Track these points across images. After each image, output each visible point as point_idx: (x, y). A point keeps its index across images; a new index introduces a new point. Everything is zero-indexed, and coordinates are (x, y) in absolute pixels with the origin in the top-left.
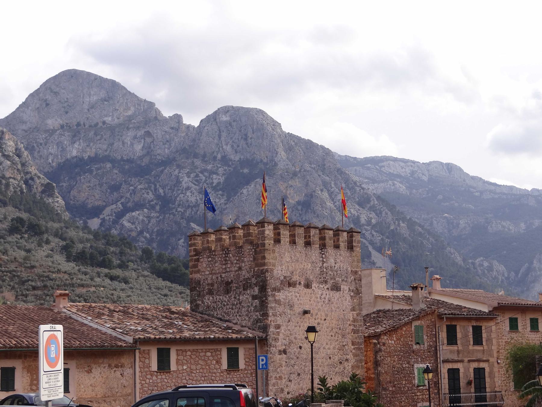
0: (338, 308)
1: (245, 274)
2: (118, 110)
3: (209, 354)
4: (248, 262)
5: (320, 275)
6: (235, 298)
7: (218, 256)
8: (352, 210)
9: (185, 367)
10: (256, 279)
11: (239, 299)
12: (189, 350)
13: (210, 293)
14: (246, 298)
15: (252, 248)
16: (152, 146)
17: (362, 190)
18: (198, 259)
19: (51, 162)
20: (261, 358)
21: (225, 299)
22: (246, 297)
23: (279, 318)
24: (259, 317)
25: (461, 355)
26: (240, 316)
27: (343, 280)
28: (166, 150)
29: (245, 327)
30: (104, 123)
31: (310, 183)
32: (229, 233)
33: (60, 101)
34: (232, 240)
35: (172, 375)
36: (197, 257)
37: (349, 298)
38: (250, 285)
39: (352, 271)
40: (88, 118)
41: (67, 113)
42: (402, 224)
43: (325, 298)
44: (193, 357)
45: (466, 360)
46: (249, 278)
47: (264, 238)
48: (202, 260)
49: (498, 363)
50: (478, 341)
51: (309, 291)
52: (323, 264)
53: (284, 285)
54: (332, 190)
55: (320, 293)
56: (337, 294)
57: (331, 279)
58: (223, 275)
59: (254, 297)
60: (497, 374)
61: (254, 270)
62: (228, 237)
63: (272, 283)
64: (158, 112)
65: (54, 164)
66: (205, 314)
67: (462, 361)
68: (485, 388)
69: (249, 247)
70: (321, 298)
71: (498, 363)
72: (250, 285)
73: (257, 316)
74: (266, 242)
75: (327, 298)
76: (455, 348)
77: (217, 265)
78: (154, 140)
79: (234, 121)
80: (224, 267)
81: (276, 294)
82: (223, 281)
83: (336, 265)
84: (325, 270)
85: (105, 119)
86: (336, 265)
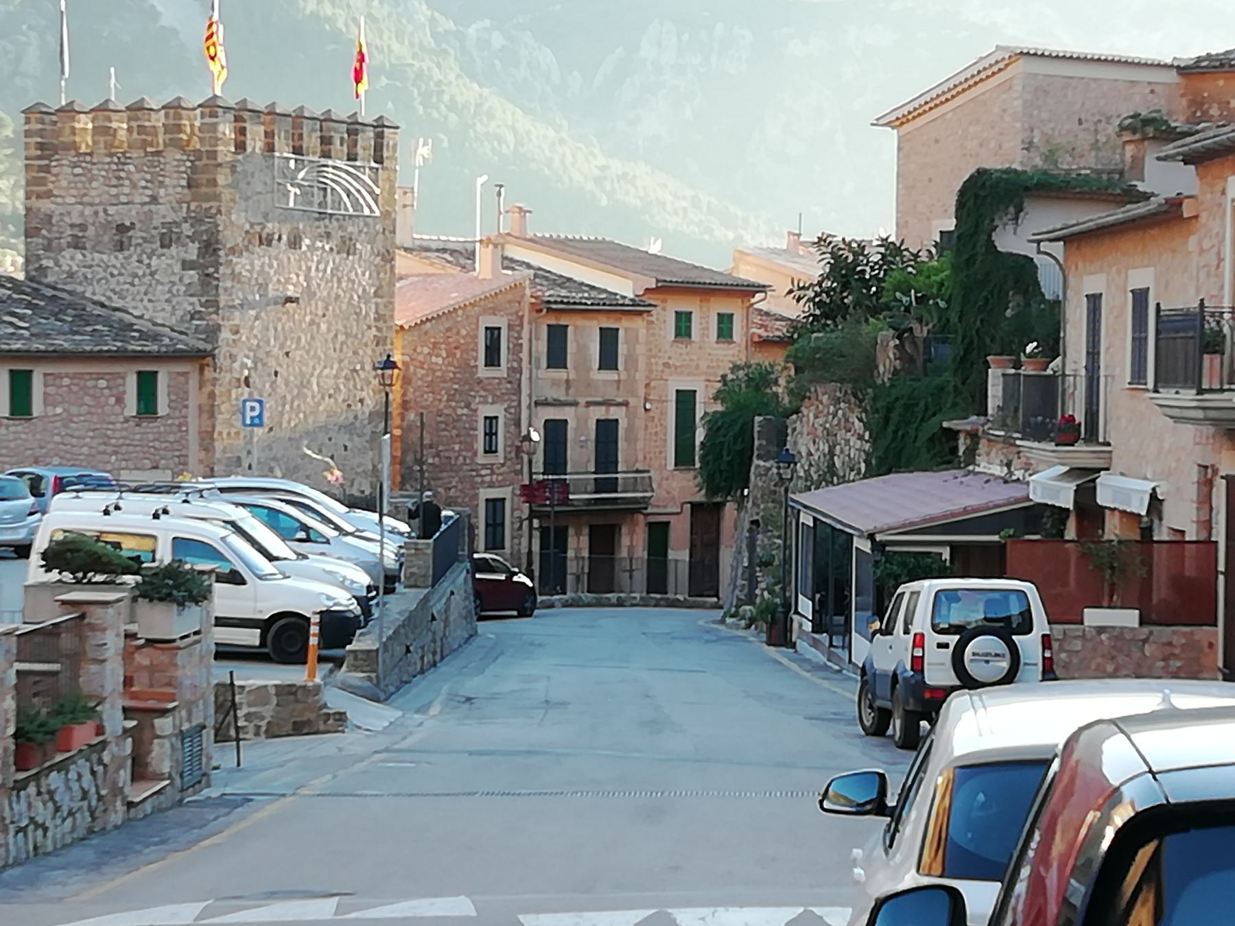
1: (164, 213)
3: (102, 383)
4: (175, 187)
6: (140, 261)
7: (100, 166)
9: (59, 410)
10: (192, 226)
11: (149, 266)
12: (67, 376)
13: (77, 244)
14: (169, 265)
15: (185, 158)
18: (48, 166)
20: (248, 404)
21: (116, 259)
22: (167, 262)
24: (199, 308)
25: (571, 391)
29: (163, 325)
32: (129, 119)
34: (135, 135)
35: (35, 424)
36: (46, 162)
44: (75, 388)
45: (582, 401)
46: (175, 222)
47: (216, 140)
49: (646, 410)
50: (608, 360)
58: (111, 210)
59: (186, 265)
60: (641, 435)
62: (125, 126)
63: (230, 236)
67: (575, 404)
68: (616, 462)
69: (178, 157)
71: (646, 410)
72: (178, 239)
73: (192, 304)
74: (220, 148)
76: (561, 374)
77: (94, 184)
80: (114, 191)
81: (235, 260)
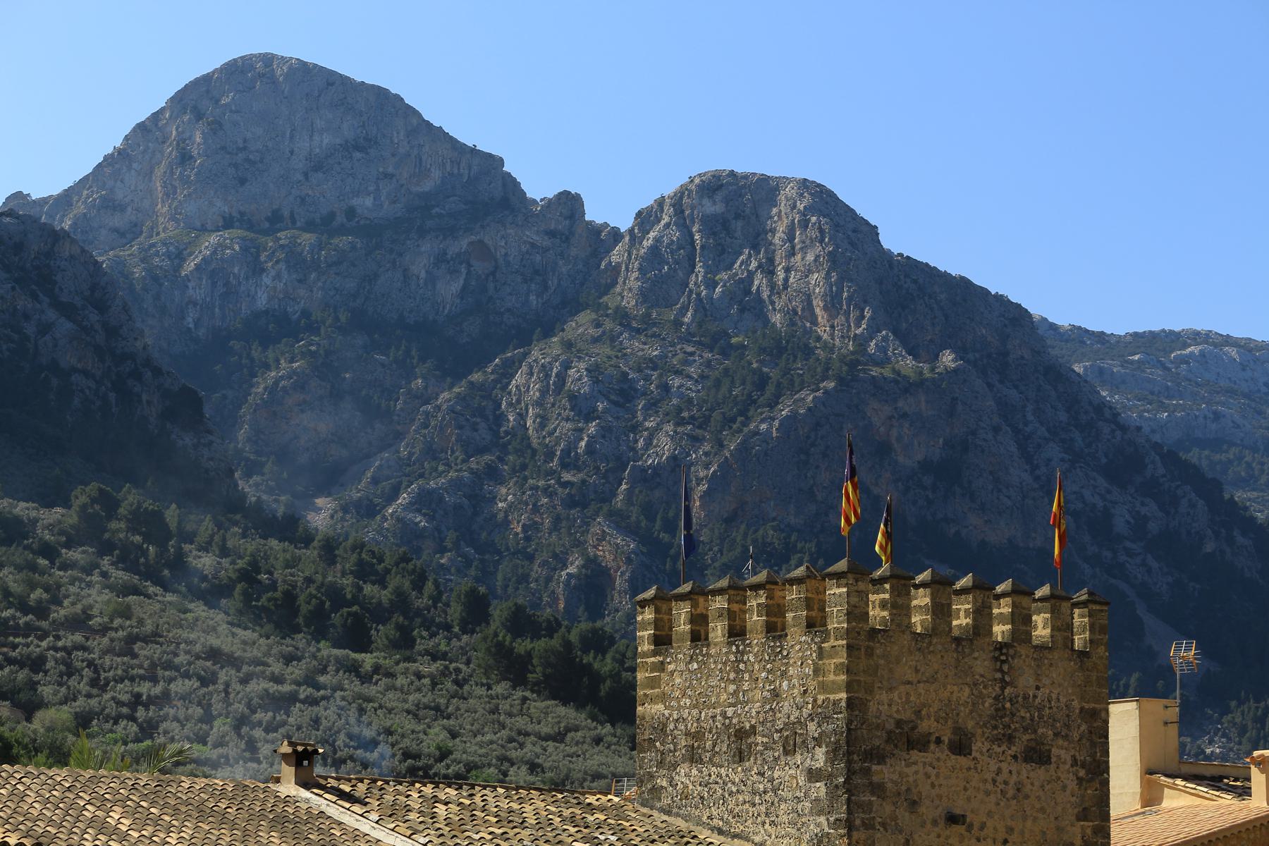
0: (1042, 810)
2: (392, 176)
5: (993, 717)
8: (1087, 493)
13: (693, 758)
16: (491, 286)
17: (1118, 433)
18: (662, 663)
19: (191, 326)
23: (879, 835)
24: (827, 830)
26: (772, 823)
27: (1056, 735)
28: (532, 297)
30: (351, 213)
31: (960, 407)
33: (223, 148)
37: (1072, 785)
38: (804, 742)
39: (1082, 709)
40: (303, 200)
41: (243, 181)
42: (1240, 540)
43: (1006, 783)
48: (671, 667)
51: (963, 761)
52: (1003, 689)
53: (896, 746)
54: (1028, 429)
55: (993, 767)
56: (1040, 773)
57: (1026, 729)
58: (730, 711)
61: (815, 701)
64: (511, 184)
65: (201, 332)
66: (678, 815)
70: (994, 781)
73: (818, 825)
75: (1012, 782)
78: (496, 267)
79: (738, 216)
80: (732, 688)
82: (728, 727)
83: (1040, 694)
84: (1008, 705)
85: (355, 202)
86: (1040, 694)
